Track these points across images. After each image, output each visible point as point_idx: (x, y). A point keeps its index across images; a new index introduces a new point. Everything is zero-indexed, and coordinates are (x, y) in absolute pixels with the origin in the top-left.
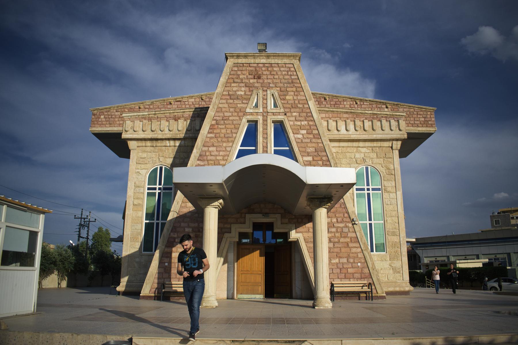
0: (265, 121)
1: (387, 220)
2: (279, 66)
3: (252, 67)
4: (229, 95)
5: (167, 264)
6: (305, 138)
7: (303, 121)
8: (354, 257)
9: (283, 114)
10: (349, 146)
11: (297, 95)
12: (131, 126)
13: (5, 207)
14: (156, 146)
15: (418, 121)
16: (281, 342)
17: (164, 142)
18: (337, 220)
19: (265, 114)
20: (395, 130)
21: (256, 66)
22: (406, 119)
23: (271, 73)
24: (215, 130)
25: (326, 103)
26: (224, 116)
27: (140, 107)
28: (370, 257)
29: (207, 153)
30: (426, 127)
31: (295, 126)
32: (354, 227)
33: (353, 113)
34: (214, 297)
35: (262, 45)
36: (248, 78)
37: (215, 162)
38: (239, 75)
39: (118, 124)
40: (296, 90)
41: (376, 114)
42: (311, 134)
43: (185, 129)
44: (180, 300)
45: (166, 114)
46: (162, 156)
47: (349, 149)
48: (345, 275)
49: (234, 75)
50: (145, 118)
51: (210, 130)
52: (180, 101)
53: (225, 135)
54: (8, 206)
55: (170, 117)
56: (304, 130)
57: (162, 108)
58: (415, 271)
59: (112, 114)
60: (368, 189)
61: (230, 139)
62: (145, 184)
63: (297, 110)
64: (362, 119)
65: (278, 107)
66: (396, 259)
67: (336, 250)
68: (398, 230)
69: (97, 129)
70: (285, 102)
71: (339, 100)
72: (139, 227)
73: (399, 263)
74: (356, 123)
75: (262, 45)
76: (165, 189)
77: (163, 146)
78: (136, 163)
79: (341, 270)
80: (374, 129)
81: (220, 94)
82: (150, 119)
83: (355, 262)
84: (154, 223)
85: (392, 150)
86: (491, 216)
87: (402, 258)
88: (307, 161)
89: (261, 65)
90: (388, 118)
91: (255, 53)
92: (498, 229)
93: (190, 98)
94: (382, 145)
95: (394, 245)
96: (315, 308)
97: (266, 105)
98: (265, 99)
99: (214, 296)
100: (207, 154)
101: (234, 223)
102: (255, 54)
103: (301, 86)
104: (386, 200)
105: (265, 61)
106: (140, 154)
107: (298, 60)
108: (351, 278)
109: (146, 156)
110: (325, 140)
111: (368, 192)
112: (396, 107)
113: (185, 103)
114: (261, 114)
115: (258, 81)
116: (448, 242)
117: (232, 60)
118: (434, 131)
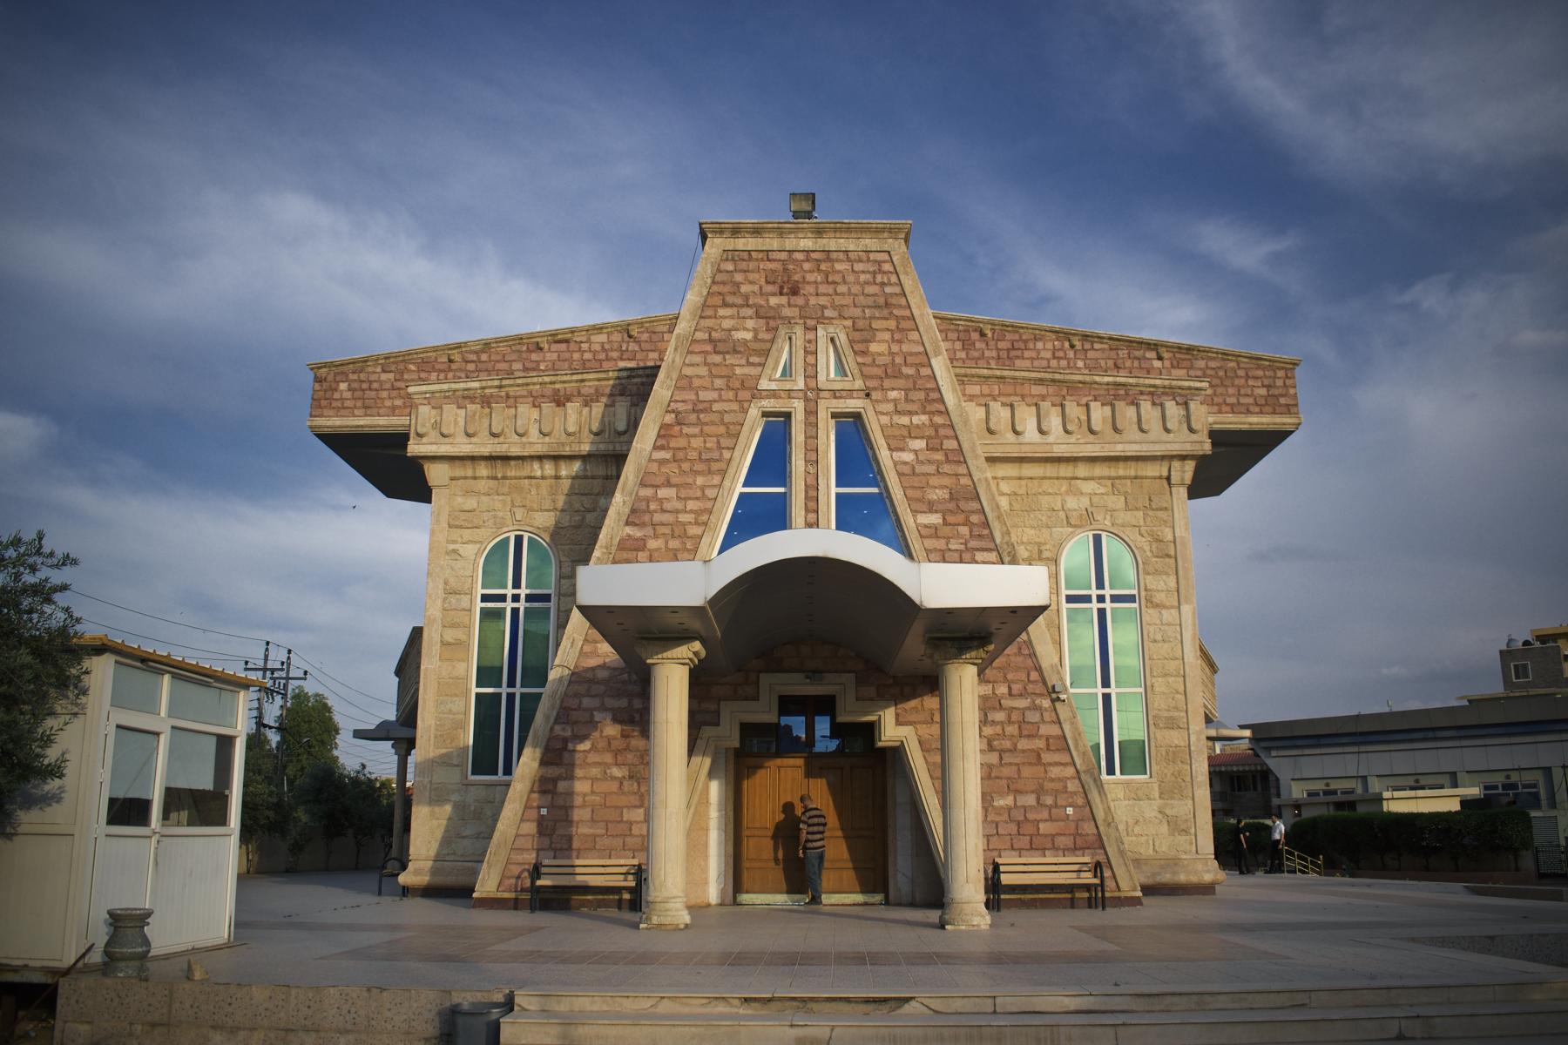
0: (811, 413)
1: (1152, 686)
3: (774, 260)
4: (711, 340)
5: (545, 810)
6: (922, 462)
7: (917, 414)
9: (862, 394)
10: (1048, 475)
11: (900, 342)
12: (433, 421)
13: (167, 678)
14: (504, 478)
16: (856, 1002)
17: (527, 465)
18: (1010, 688)
19: (812, 396)
20: (1179, 429)
21: (786, 258)
22: (1215, 391)
23: (827, 277)
24: (673, 439)
25: (983, 346)
29: (651, 503)
30: (1272, 413)
32: (1055, 709)
33: (1059, 381)
34: (681, 900)
35: (803, 198)
36: (764, 291)
37: (675, 528)
38: (738, 285)
39: (389, 407)
41: (1124, 385)
43: (584, 428)
44: (583, 909)
45: (531, 387)
46: (521, 504)
47: (1047, 485)
48: (1031, 840)
49: (723, 283)
50: (472, 399)
51: (659, 440)
52: (567, 341)
53: (700, 453)
54: (174, 676)
55: (543, 396)
56: (919, 441)
57: (515, 361)
58: (1259, 823)
59: (373, 377)
60: (1101, 599)
61: (715, 466)
62: (474, 586)
63: (901, 383)
64: (1084, 401)
65: (846, 376)
66: (1179, 796)
67: (1006, 771)
68: (1183, 714)
69: (329, 423)
70: (868, 360)
71: (1020, 336)
72: (459, 706)
73: (1186, 805)
74: (1067, 410)
75: (803, 198)
76: (529, 598)
77: (525, 478)
78: (450, 526)
79: (1019, 828)
80: (1118, 427)
81: (687, 340)
82: (486, 402)
83: (1059, 803)
84: (500, 695)
85: (1170, 487)
86: (1501, 652)
87: (1195, 792)
89: (800, 256)
91: (781, 223)
92: (1517, 694)
93: (596, 332)
94: (1140, 473)
95: (1171, 754)
96: (945, 929)
97: (815, 368)
98: (812, 353)
99: (680, 897)
100: (653, 506)
101: (727, 699)
102: (783, 225)
103: (912, 315)
105: (810, 243)
106: (460, 500)
107: (903, 241)
108: (1048, 849)
109: (475, 506)
111: (1101, 605)
112: (1187, 357)
113: (580, 348)
114: (801, 394)
115: (792, 302)
116: (1362, 734)
117: (718, 241)
118: (1293, 424)
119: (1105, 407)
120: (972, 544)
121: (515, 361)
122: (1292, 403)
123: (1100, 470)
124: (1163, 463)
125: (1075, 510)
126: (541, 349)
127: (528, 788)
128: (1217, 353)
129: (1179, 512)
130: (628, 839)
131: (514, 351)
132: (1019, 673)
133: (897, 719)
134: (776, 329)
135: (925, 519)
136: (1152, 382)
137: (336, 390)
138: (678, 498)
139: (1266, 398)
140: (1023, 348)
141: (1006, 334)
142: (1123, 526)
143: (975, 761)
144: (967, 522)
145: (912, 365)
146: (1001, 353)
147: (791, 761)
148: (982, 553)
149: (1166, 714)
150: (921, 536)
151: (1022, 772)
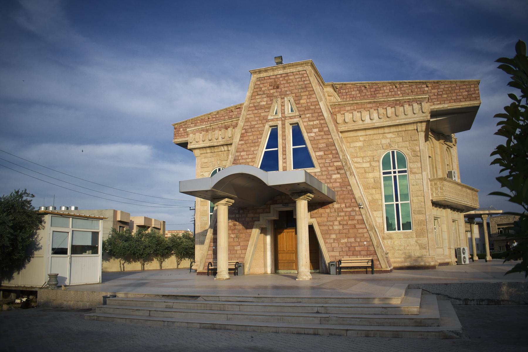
0: (283, 124)
2: (294, 75)
3: (272, 79)
7: (315, 121)
8: (361, 237)
9: (299, 116)
10: (375, 133)
13: (71, 219)
14: (214, 152)
15: (460, 95)
17: (220, 148)
18: (346, 205)
20: (419, 113)
21: (275, 77)
22: (448, 96)
24: (245, 137)
25: (366, 91)
26: (251, 125)
27: (209, 117)
28: (375, 237)
30: (470, 101)
31: (308, 126)
32: (360, 211)
33: (376, 102)
38: (261, 88)
40: (309, 94)
41: (397, 100)
42: (322, 131)
45: (219, 125)
47: (375, 137)
49: (257, 88)
50: (203, 130)
55: (222, 127)
56: (316, 129)
57: (226, 116)
60: (395, 172)
61: (256, 144)
63: (310, 111)
64: (385, 107)
65: (294, 112)
68: (424, 209)
69: (178, 140)
70: (300, 106)
71: (378, 86)
73: (425, 239)
74: (379, 111)
78: (201, 168)
79: (349, 249)
81: (247, 107)
83: (362, 241)
88: (319, 156)
89: (279, 76)
90: (410, 103)
95: (420, 223)
96: (296, 280)
100: (240, 158)
104: (412, 181)
105: (282, 71)
106: (203, 160)
110: (334, 135)
117: (255, 75)
119: (392, 108)
120: (333, 160)
121: (226, 116)
122: (477, 96)
123: (393, 129)
124: (414, 125)
125: (385, 144)
126: (232, 111)
127: (210, 241)
128: (448, 82)
129: (421, 141)
130: (236, 255)
131: (225, 113)
132: (349, 200)
133: (311, 216)
134: (272, 100)
135: (318, 154)
136: (408, 98)
137: (179, 131)
138: (247, 155)
139: (467, 95)
140: (379, 90)
141: (373, 86)
142: (402, 147)
143: (305, 229)
144: (331, 153)
145: (313, 105)
146: (372, 93)
147: (291, 230)
148: (336, 163)
149: (417, 209)
150: (317, 159)
151: (350, 231)
